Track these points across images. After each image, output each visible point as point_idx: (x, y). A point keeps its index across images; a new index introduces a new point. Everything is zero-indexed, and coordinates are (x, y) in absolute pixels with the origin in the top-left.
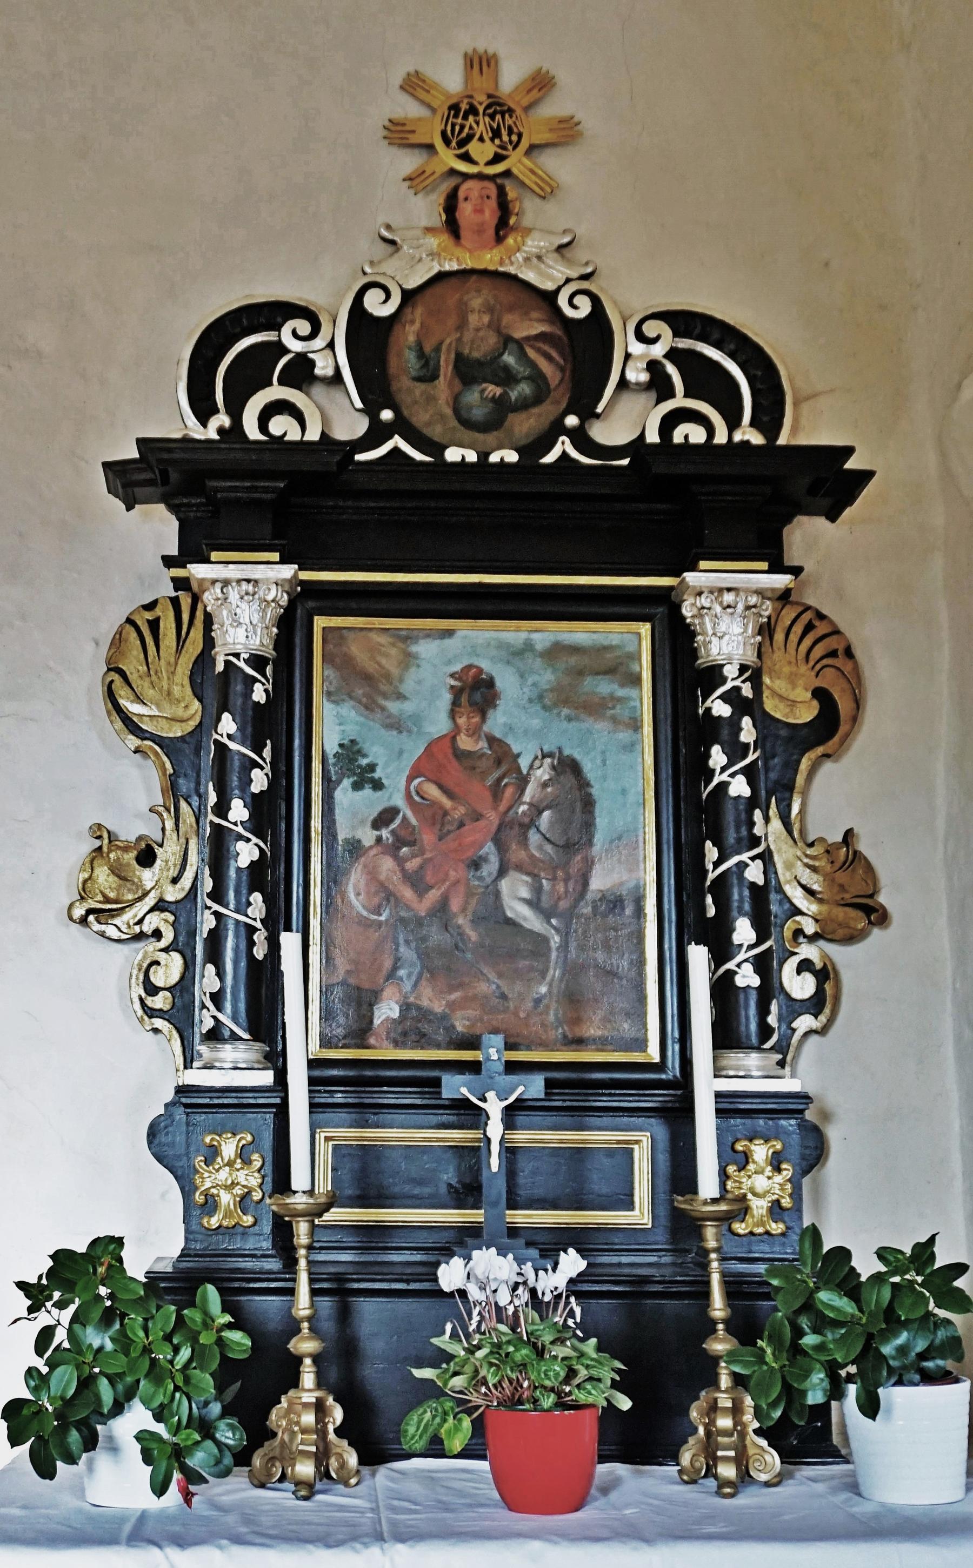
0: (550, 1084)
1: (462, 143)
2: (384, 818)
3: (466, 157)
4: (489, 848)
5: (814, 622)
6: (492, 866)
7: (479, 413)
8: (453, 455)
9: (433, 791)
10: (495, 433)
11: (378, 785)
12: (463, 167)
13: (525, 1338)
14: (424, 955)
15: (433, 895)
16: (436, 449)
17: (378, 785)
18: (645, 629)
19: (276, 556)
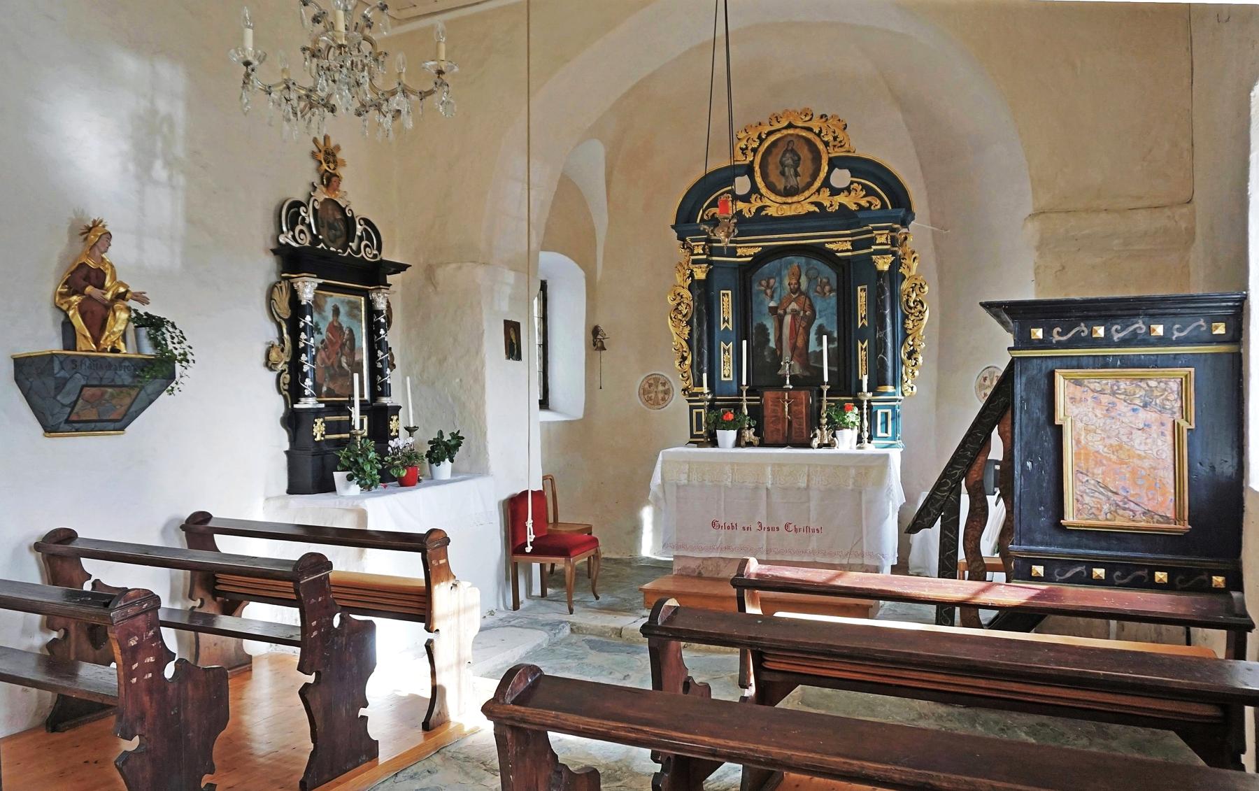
0: (326, 406)
1: (328, 163)
2: (323, 341)
3: (329, 167)
4: (339, 350)
5: (1240, 593)
6: (340, 354)
7: (332, 238)
8: (332, 249)
9: (330, 335)
10: (1156, 625)
11: (321, 334)
12: (328, 169)
13: (825, 338)
14: (329, 375)
15: (331, 361)
16: (328, 247)
17: (321, 334)
18: (363, 298)
19: (315, 276)
